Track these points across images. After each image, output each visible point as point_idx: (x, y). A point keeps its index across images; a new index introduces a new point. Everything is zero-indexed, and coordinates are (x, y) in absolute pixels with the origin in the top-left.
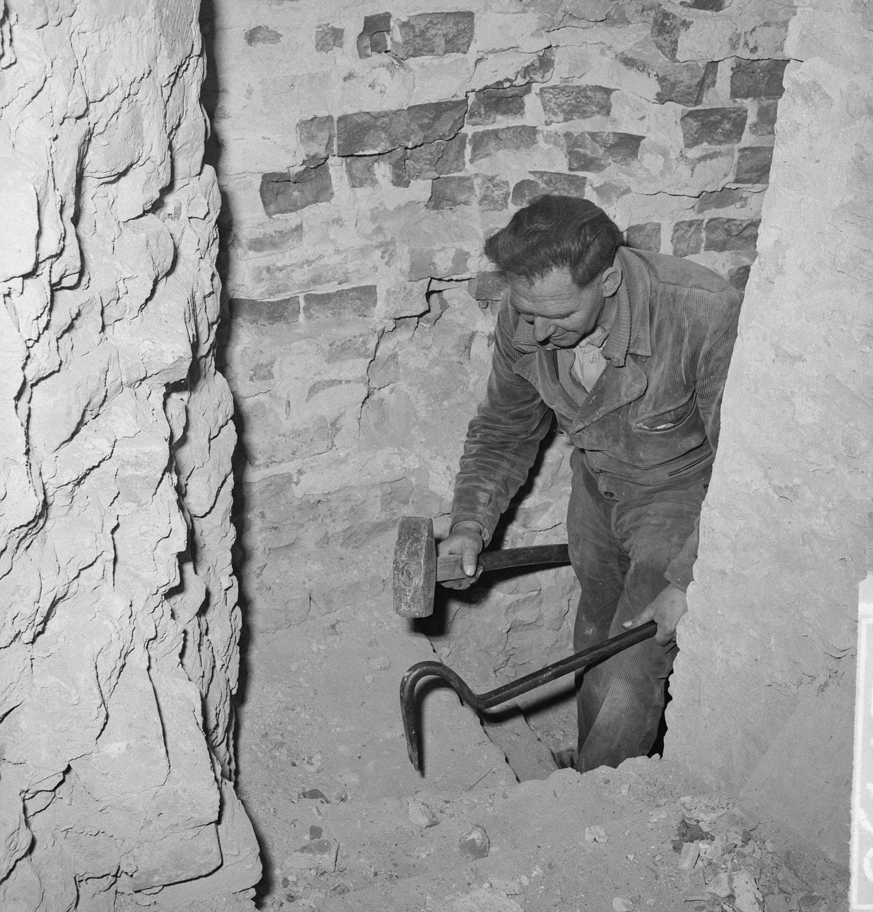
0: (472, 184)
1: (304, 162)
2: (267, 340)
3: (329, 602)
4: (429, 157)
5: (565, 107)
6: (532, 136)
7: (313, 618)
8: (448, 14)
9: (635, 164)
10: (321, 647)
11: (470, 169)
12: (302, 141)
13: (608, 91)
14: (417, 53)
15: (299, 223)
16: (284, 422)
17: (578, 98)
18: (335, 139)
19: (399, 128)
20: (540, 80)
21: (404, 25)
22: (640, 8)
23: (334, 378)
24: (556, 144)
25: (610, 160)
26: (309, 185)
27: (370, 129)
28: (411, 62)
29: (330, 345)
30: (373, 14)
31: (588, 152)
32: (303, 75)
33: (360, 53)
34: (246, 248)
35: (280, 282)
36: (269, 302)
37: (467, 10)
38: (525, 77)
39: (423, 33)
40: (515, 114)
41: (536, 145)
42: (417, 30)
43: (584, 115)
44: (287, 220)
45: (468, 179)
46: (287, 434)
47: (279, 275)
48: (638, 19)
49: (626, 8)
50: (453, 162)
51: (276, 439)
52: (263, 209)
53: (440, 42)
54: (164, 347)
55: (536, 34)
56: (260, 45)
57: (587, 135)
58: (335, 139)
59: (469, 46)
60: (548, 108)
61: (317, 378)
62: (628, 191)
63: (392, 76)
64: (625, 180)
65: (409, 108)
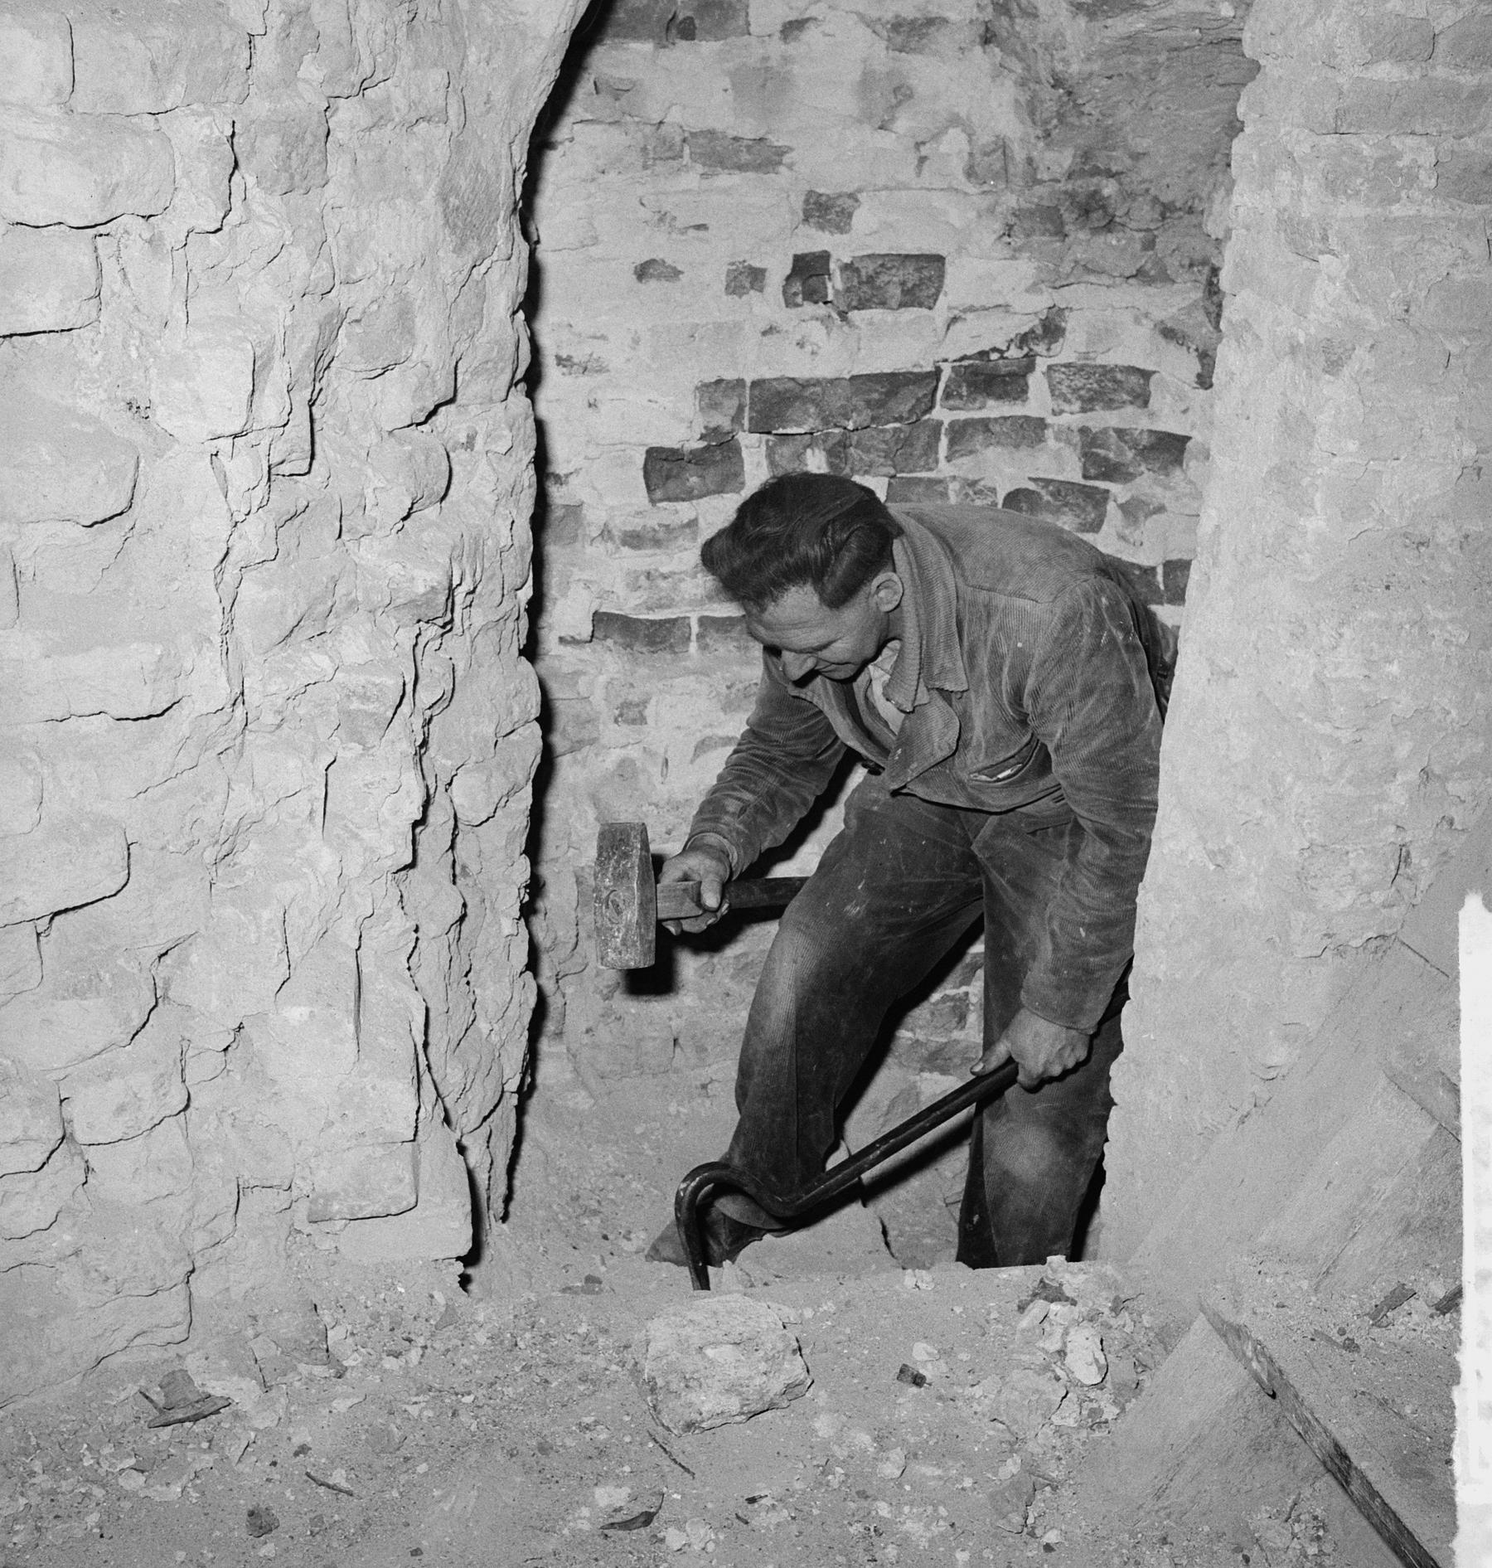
0: (946, 488)
1: (702, 437)
2: (643, 671)
3: (701, 1049)
4: (884, 446)
5: (1082, 392)
6: (1039, 431)
7: (676, 1071)
8: (907, 256)
9: (1177, 473)
10: (681, 1109)
11: (944, 469)
12: (701, 409)
13: (1146, 375)
14: (862, 305)
15: (693, 517)
16: (659, 786)
17: (1102, 381)
18: (747, 409)
19: (835, 403)
20: (1045, 353)
21: (846, 268)
22: (1186, 262)
23: (730, 735)
24: (1068, 442)
25: (1143, 468)
26: (712, 470)
27: (795, 401)
28: (854, 315)
29: (728, 687)
30: (806, 251)
31: (1111, 455)
32: (707, 324)
33: (786, 301)
34: (618, 542)
35: (663, 594)
36: (648, 620)
37: (934, 252)
38: (1021, 348)
39: (871, 280)
40: (1015, 399)
41: (1043, 444)
42: (863, 273)
43: (1110, 405)
44: (677, 512)
45: (940, 481)
46: (662, 803)
47: (663, 584)
48: (1186, 277)
49: (1168, 261)
50: (920, 457)
51: (644, 809)
52: (646, 494)
53: (895, 292)
54: (416, 573)
55: (1033, 288)
56: (653, 284)
57: (1112, 433)
58: (747, 409)
59: (935, 300)
60: (1057, 393)
61: (708, 732)
62: (1161, 509)
63: (828, 334)
64: (1159, 494)
65: (853, 378)
